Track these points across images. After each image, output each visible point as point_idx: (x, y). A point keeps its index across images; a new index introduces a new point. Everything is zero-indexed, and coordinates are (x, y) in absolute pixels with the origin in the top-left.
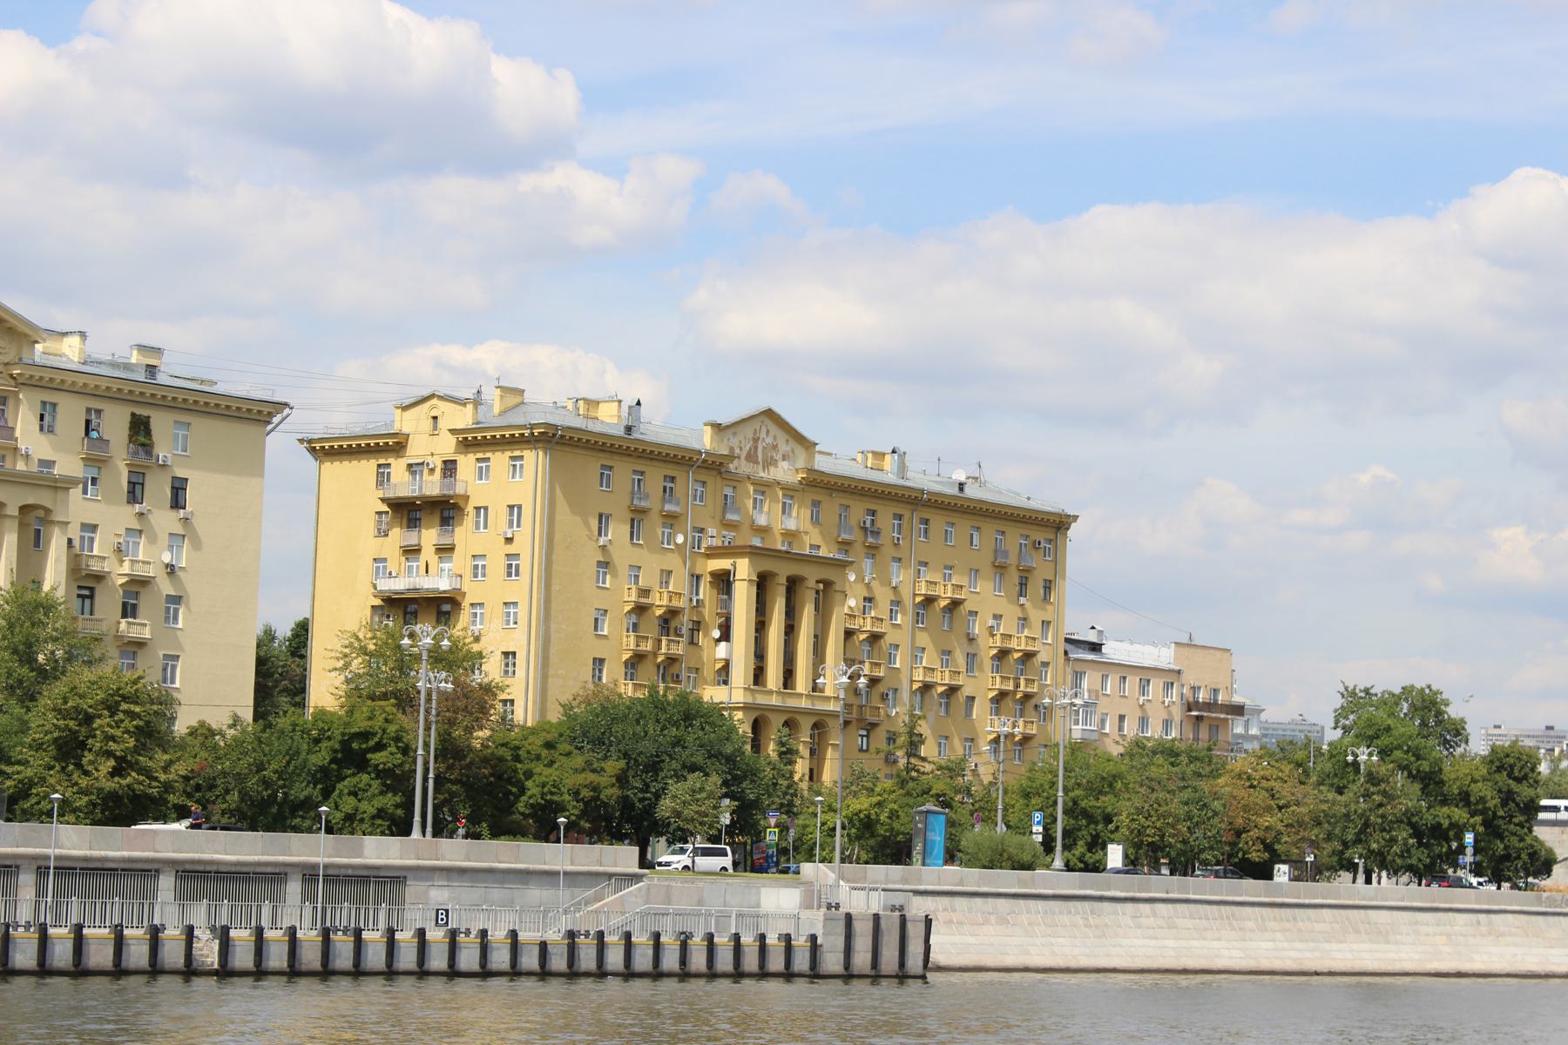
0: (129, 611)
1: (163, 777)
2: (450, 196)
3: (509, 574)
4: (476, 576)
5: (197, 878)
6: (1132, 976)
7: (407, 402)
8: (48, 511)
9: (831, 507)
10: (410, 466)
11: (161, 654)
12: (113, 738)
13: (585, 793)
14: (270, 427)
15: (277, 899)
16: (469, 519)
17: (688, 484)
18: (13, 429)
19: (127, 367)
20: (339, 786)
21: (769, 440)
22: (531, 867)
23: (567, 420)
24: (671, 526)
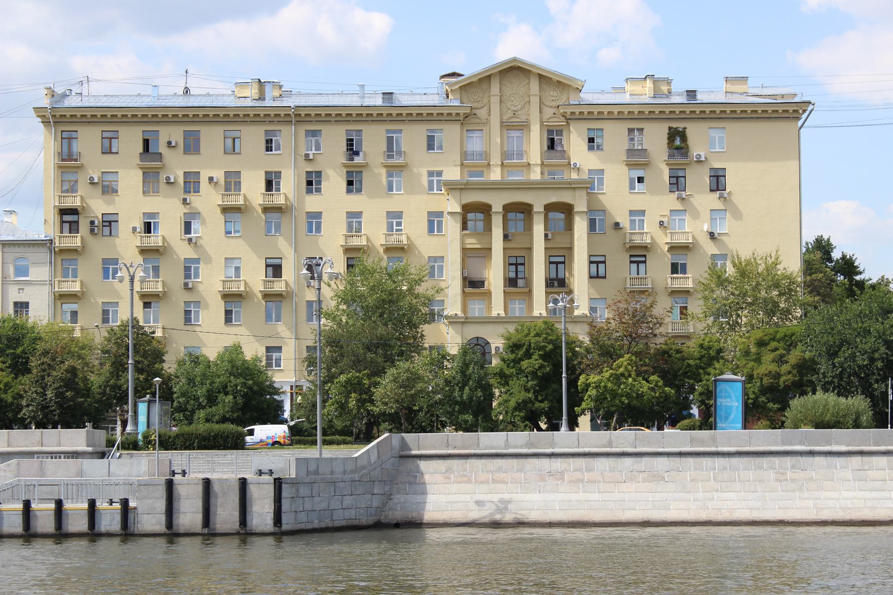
6: (769, 529)
14: (800, 123)
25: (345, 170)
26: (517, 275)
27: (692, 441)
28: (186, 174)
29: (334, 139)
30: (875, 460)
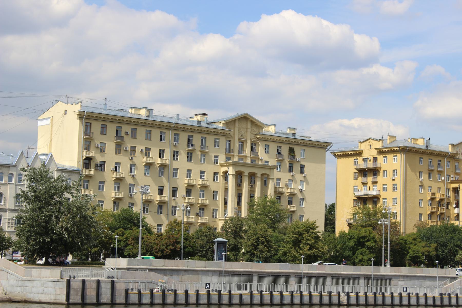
0: (290, 202)
1: (322, 250)
2: (342, 76)
3: (394, 190)
4: (384, 190)
5: (336, 278)
7: (362, 141)
8: (268, 175)
10: (363, 159)
11: (299, 214)
12: (308, 240)
13: (426, 253)
15: (288, 283)
16: (382, 174)
17: (445, 162)
18: (258, 152)
19: (287, 134)
20: (357, 252)
22: (426, 275)
23: (409, 144)
24: (440, 175)
25: (187, 152)
28: (131, 146)
29: (183, 137)
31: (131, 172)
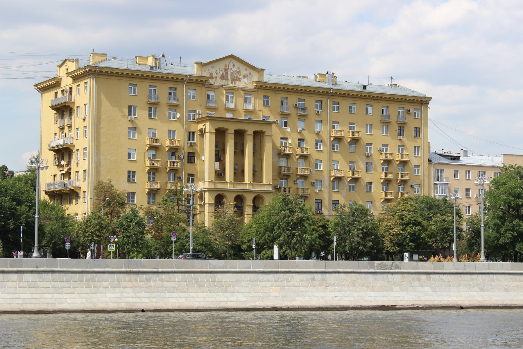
9: (275, 99)
21: (235, 69)
26: (178, 203)
27: (378, 267)
30: (11, 276)
31: (317, 148)
